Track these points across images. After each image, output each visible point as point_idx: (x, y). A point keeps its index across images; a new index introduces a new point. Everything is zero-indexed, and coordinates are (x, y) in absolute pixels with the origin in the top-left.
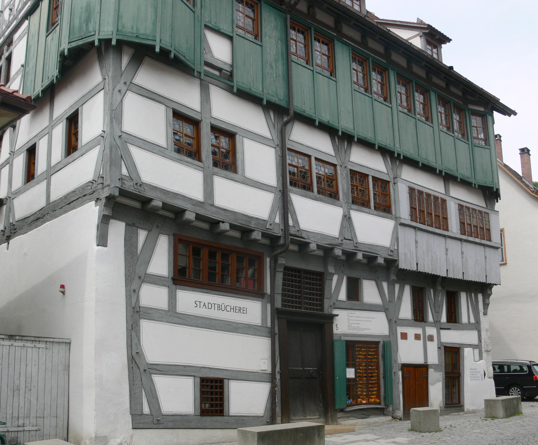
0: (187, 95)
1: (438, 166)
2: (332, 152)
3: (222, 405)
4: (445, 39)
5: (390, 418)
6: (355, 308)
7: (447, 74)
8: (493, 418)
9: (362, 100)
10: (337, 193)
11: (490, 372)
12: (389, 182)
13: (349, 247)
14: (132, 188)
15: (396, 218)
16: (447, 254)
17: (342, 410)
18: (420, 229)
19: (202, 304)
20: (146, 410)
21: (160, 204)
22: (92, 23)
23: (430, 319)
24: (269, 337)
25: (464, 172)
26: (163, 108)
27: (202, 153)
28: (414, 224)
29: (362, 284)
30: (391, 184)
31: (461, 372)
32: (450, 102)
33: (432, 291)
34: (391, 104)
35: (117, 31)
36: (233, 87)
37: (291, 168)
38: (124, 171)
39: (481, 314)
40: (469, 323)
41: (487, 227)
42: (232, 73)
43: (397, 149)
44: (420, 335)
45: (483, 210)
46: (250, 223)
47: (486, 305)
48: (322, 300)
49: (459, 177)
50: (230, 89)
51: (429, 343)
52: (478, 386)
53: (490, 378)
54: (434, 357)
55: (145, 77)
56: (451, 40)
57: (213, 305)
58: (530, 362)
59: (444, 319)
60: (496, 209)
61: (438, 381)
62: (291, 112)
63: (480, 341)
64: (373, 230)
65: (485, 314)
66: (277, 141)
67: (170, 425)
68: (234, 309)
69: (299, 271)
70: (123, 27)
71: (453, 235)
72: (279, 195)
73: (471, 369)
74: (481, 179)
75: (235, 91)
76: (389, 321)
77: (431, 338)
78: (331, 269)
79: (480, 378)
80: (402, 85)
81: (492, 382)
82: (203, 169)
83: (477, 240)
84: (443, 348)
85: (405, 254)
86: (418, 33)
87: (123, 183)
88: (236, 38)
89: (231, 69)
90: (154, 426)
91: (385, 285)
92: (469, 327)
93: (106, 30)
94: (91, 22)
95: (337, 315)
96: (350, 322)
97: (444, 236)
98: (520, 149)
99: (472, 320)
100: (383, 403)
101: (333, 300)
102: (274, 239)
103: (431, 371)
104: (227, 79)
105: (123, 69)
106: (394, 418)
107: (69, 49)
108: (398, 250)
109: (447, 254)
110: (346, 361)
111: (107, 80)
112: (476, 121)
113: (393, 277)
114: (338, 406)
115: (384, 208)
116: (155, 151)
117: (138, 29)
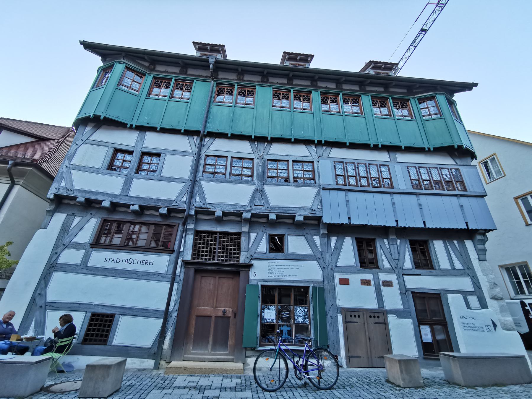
7: (441, 85)
18: (350, 190)
19: (111, 260)
21: (83, 199)
37: (298, 166)
40: (454, 268)
44: (370, 280)
51: (385, 290)
57: (121, 260)
59: (408, 264)
68: (141, 262)
69: (215, 233)
77: (388, 284)
91: (317, 239)
96: (272, 269)
103: (392, 319)
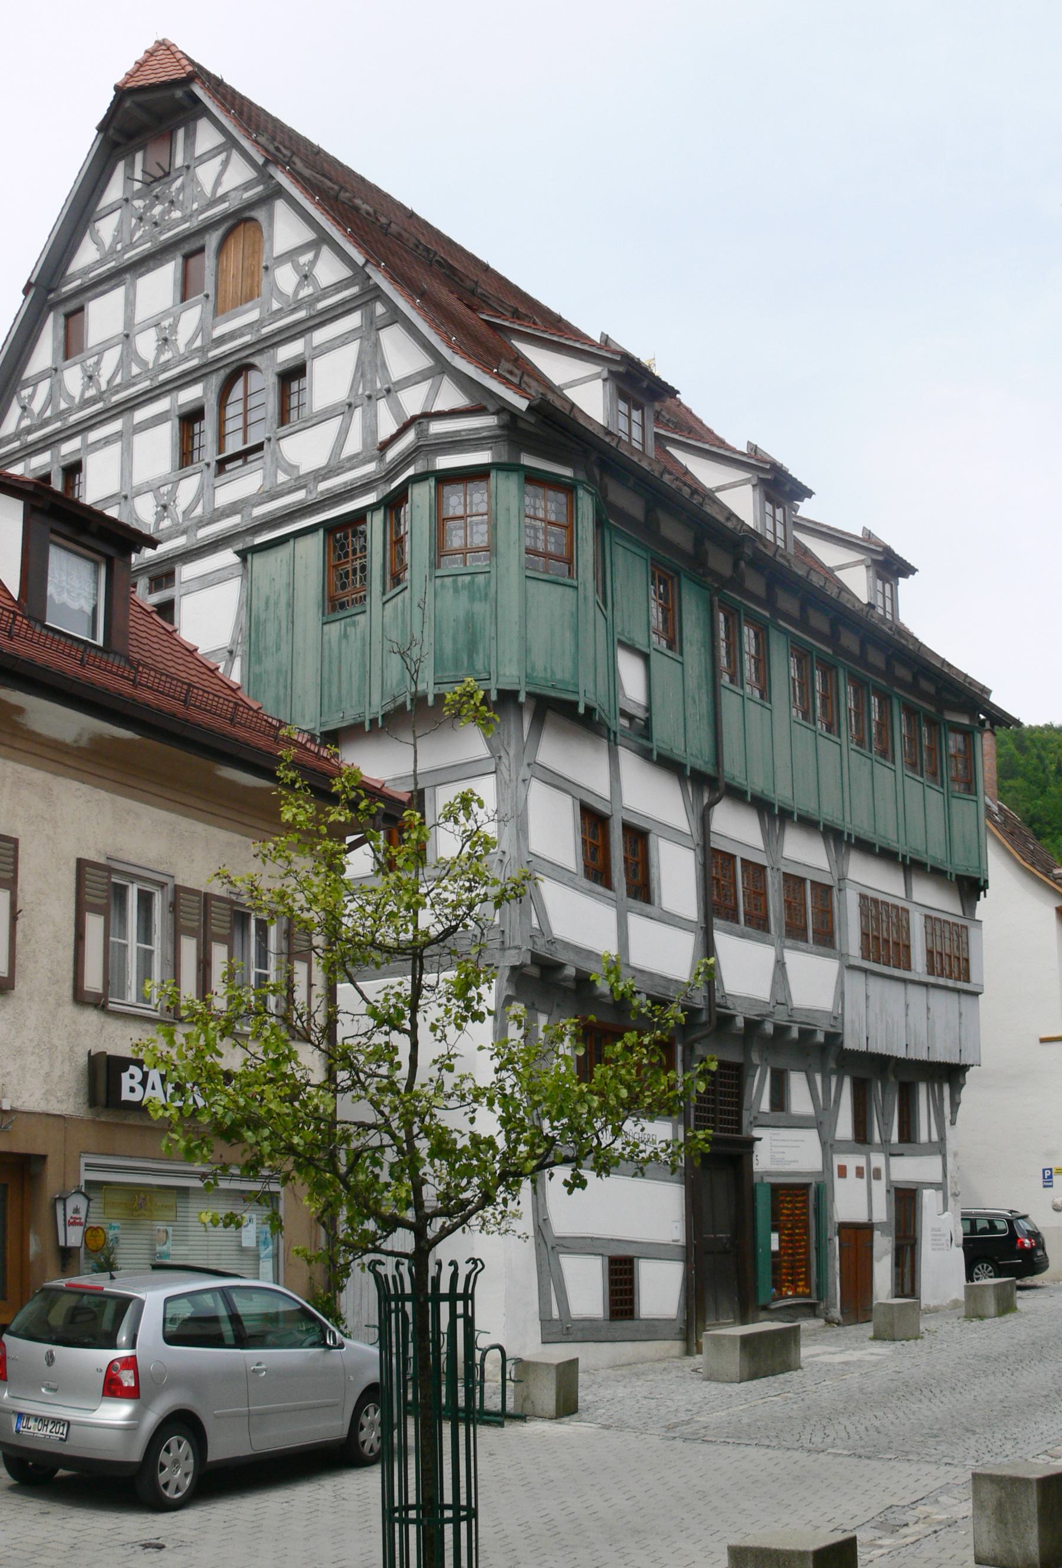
0: (587, 766)
1: (901, 848)
2: (760, 843)
3: (631, 1302)
4: (906, 570)
5: (822, 1322)
6: (780, 1124)
8: (981, 1317)
9: (804, 735)
10: (766, 919)
11: (959, 1231)
12: (830, 887)
13: (781, 1018)
14: (544, 949)
15: (842, 956)
16: (907, 1015)
17: (765, 1308)
20: (556, 1314)
22: (481, 656)
23: (877, 1138)
24: (681, 1183)
25: (935, 853)
26: (569, 799)
27: (613, 875)
28: (866, 965)
29: (788, 1079)
30: (835, 891)
31: (918, 1234)
32: (919, 713)
33: (879, 1085)
34: (839, 737)
35: (526, 677)
36: (651, 750)
38: (535, 923)
39: (947, 1123)
41: (965, 956)
42: (648, 722)
43: (847, 827)
44: (862, 1168)
45: (960, 921)
46: (668, 989)
47: (955, 1105)
48: (739, 1114)
49: (929, 862)
50: (646, 754)
51: (874, 1182)
52: (942, 1265)
53: (958, 1246)
54: (881, 1212)
55: (555, 751)
56: (917, 570)
58: (1011, 1212)
59: (895, 1137)
60: (977, 918)
61: (885, 1253)
62: (721, 784)
63: (945, 1175)
64: (813, 983)
65: (953, 1123)
66: (697, 838)
67: (579, 1336)
70: (533, 669)
71: (916, 978)
72: (701, 933)
73: (933, 1229)
74: (960, 865)
75: (655, 757)
76: (823, 1144)
78: (755, 1059)
80: (913, 765)
81: (961, 1250)
82: (616, 903)
83: (950, 983)
84: (893, 1191)
85: (853, 1022)
86: (862, 557)
87: (534, 942)
88: (654, 656)
89: (647, 715)
90: (565, 1338)
93: (508, 674)
94: (477, 653)
95: (760, 1139)
96: (774, 1149)
97: (904, 981)
99: (935, 1137)
100: (814, 1295)
101: (754, 1113)
102: (692, 1012)
103: (877, 1234)
104: (640, 735)
105: (525, 738)
106: (829, 1322)
108: (843, 1015)
109: (907, 1015)
110: (773, 1220)
111: (504, 760)
112: (954, 742)
113: (832, 1065)
114: (762, 1301)
115: (825, 939)
116: (565, 880)
117: (553, 672)
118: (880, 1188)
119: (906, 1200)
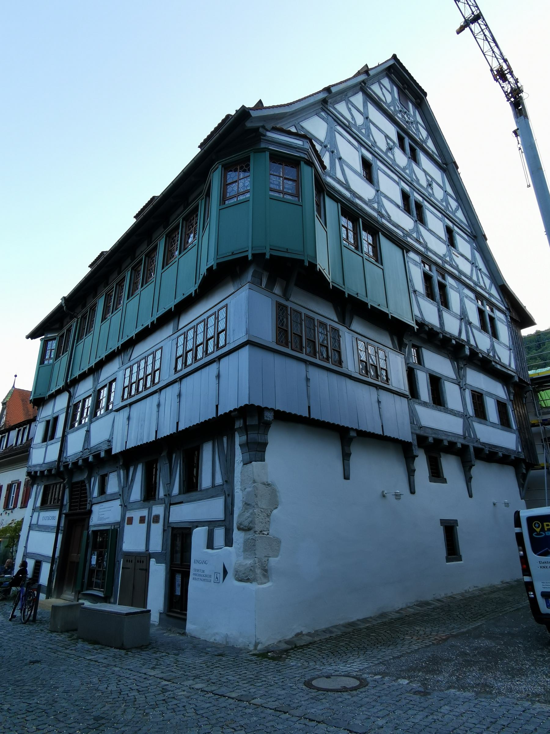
4: (260, 102)
23: (161, 493)
44: (153, 522)
51: (153, 526)
77: (156, 519)
79: (212, 579)
92: (213, 492)
98: (394, 57)
99: (219, 480)
107: (217, 264)
118: (157, 529)
119: (179, 539)
